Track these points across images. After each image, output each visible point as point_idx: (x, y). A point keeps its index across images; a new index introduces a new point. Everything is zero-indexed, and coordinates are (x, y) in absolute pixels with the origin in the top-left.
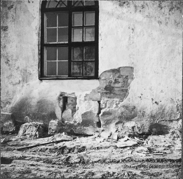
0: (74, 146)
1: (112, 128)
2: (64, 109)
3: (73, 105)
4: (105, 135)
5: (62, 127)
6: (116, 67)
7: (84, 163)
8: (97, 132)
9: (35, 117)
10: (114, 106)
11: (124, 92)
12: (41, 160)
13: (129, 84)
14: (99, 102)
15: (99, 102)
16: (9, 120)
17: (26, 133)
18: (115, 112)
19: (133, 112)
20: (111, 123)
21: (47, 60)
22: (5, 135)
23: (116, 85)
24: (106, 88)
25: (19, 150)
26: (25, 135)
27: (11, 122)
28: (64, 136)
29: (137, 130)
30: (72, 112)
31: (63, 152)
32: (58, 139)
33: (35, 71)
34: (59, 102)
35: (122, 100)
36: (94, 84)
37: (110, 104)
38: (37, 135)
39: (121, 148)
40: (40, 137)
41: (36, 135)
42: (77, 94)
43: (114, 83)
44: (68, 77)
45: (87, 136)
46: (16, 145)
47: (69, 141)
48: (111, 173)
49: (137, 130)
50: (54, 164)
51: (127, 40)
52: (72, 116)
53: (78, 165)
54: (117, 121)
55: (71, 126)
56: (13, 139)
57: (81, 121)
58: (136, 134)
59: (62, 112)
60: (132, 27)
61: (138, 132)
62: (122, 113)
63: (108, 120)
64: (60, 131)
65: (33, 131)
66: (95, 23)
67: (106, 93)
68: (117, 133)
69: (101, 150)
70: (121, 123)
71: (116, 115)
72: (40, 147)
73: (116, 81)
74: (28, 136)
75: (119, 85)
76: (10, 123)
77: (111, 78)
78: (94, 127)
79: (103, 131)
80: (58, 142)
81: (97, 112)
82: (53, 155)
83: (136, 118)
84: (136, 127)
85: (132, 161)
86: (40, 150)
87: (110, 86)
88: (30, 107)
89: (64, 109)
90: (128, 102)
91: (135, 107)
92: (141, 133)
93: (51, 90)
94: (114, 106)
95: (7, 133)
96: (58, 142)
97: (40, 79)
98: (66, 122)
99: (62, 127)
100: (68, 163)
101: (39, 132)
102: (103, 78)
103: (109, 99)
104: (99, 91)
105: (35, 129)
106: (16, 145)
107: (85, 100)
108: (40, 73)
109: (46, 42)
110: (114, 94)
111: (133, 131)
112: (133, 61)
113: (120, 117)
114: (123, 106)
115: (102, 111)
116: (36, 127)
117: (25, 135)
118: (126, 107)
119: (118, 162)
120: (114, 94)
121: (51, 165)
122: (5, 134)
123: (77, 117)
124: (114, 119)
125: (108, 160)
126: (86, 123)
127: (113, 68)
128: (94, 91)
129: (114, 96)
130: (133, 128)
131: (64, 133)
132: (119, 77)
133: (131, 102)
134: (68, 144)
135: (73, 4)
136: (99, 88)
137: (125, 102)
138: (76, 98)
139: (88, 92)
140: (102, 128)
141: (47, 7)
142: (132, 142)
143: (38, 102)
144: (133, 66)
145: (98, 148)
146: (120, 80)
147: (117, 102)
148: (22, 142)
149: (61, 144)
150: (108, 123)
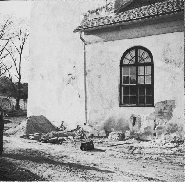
0: (138, 146)
1: (163, 136)
2: (134, 124)
3: (139, 122)
4: (158, 141)
5: (133, 135)
6: (165, 100)
7: (140, 154)
8: (154, 139)
9: (117, 129)
10: (164, 124)
11: (170, 116)
12: (119, 151)
13: (173, 110)
14: (155, 121)
15: (155, 121)
16: (103, 129)
17: (112, 138)
18: (164, 127)
19: (175, 128)
20: (162, 134)
21: (124, 94)
22: (101, 139)
23: (165, 111)
24: (159, 112)
25: (108, 146)
26: (112, 139)
27: (104, 131)
28: (133, 140)
29: (177, 139)
30: (139, 127)
31: (131, 149)
32: (130, 142)
33: (117, 102)
34: (131, 120)
35: (169, 120)
36: (149, 111)
37: (161, 122)
38: (118, 139)
39: (164, 148)
40: (120, 140)
41: (118, 139)
42: (142, 116)
43: (164, 110)
44: (136, 105)
45: (148, 141)
46: (107, 144)
47: (136, 143)
48: (150, 157)
49: (177, 139)
50: (126, 153)
51: (171, 84)
52: (139, 129)
53: (137, 154)
54: (166, 133)
55: (138, 135)
56: (105, 141)
57: (144, 132)
58: (176, 141)
59: (133, 126)
60: (174, 76)
61: (178, 140)
62: (169, 128)
63: (160, 132)
64: (132, 138)
65: (116, 137)
66: (152, 73)
67: (159, 116)
68: (165, 140)
69: (152, 149)
70: (168, 134)
71: (165, 129)
72: (119, 146)
73: (165, 109)
74: (114, 140)
75: (167, 111)
76: (103, 132)
77: (162, 106)
78: (152, 136)
79: (157, 138)
80: (130, 144)
81: (153, 127)
82: (126, 150)
83: (177, 131)
84: (177, 137)
85: (165, 154)
86: (120, 147)
87: (161, 111)
88: (114, 122)
89: (134, 124)
90: (172, 122)
91: (176, 125)
92: (179, 140)
93: (128, 112)
94: (164, 123)
95: (102, 137)
96: (130, 144)
97: (119, 106)
98: (135, 132)
99: (133, 135)
100: (133, 154)
101: (120, 137)
102: (157, 107)
103: (161, 119)
104: (155, 114)
105: (117, 136)
106: (107, 144)
107: (146, 119)
108: (119, 103)
109: (123, 84)
110: (164, 116)
111: (175, 139)
112: (175, 97)
113: (167, 131)
114: (169, 124)
115: (157, 127)
116: (118, 134)
117: (112, 139)
118: (171, 125)
119: (158, 154)
120: (164, 116)
121: (124, 154)
122: (100, 138)
123: (141, 130)
124: (164, 131)
125: (153, 153)
126: (147, 133)
127: (163, 101)
128: (151, 114)
129: (164, 118)
130: (175, 137)
131: (134, 139)
132: (166, 106)
133: (174, 122)
134: (135, 145)
135: (138, 61)
136: (154, 113)
137: (171, 121)
138: (141, 118)
139: (148, 115)
140: (157, 137)
141: (123, 63)
142: (172, 145)
143: (119, 120)
144: (175, 100)
145: (151, 148)
146: (167, 108)
147: (166, 122)
148: (110, 143)
149: (131, 145)
150: (160, 134)
